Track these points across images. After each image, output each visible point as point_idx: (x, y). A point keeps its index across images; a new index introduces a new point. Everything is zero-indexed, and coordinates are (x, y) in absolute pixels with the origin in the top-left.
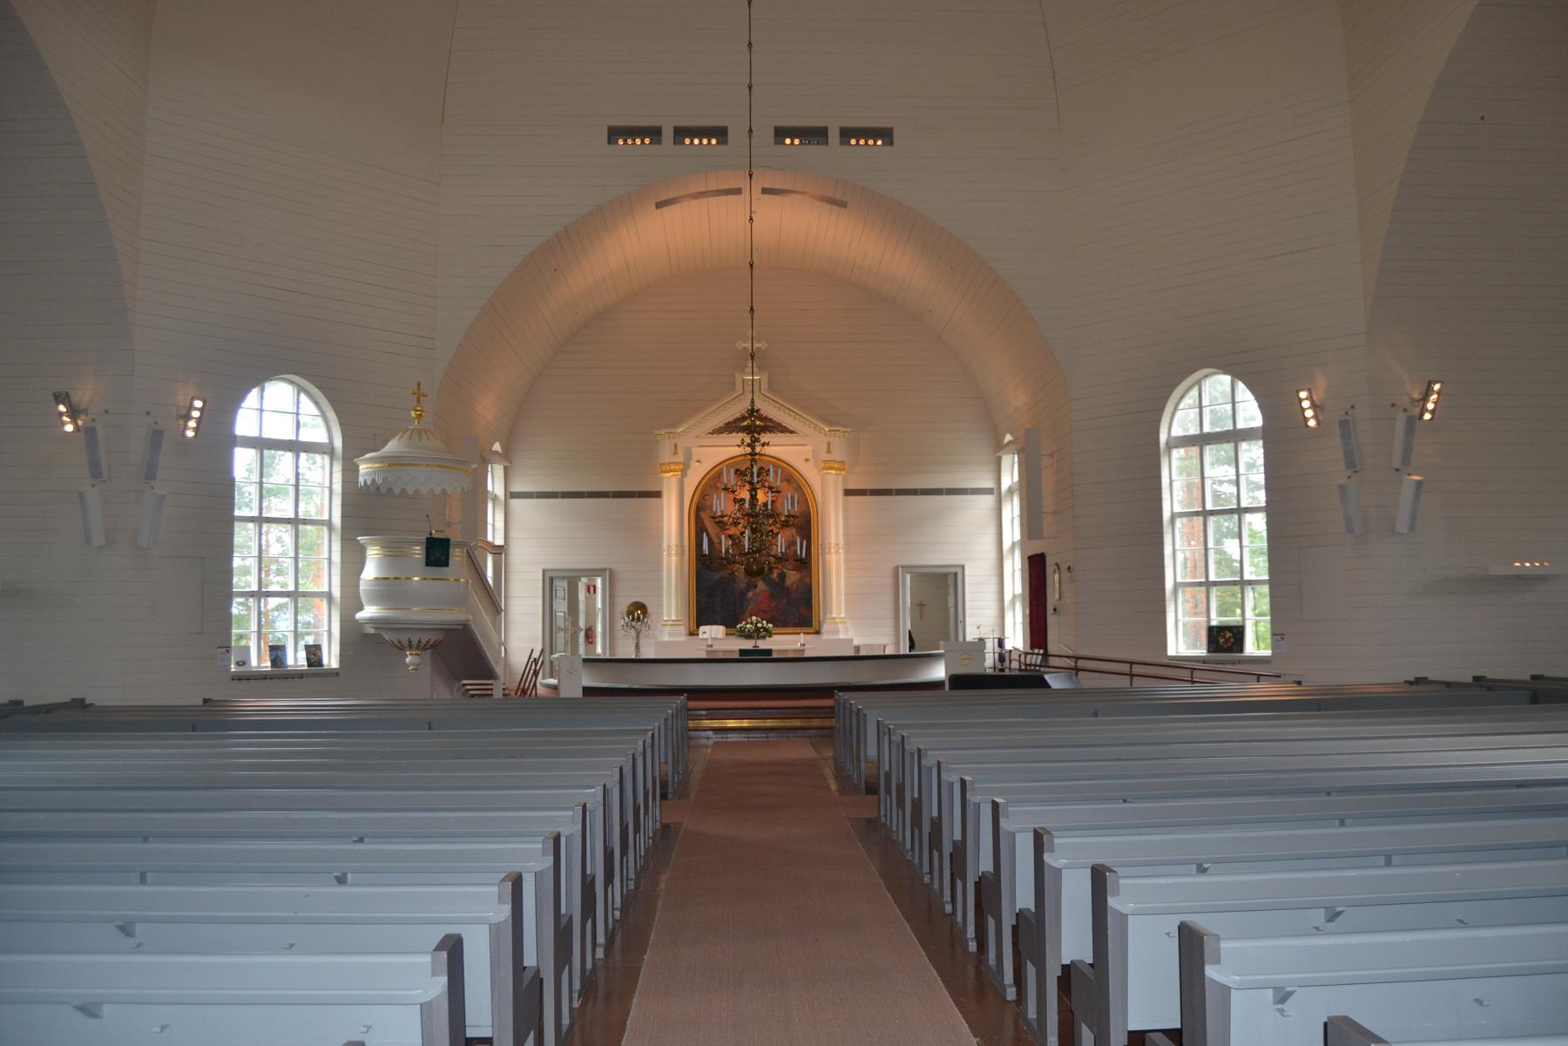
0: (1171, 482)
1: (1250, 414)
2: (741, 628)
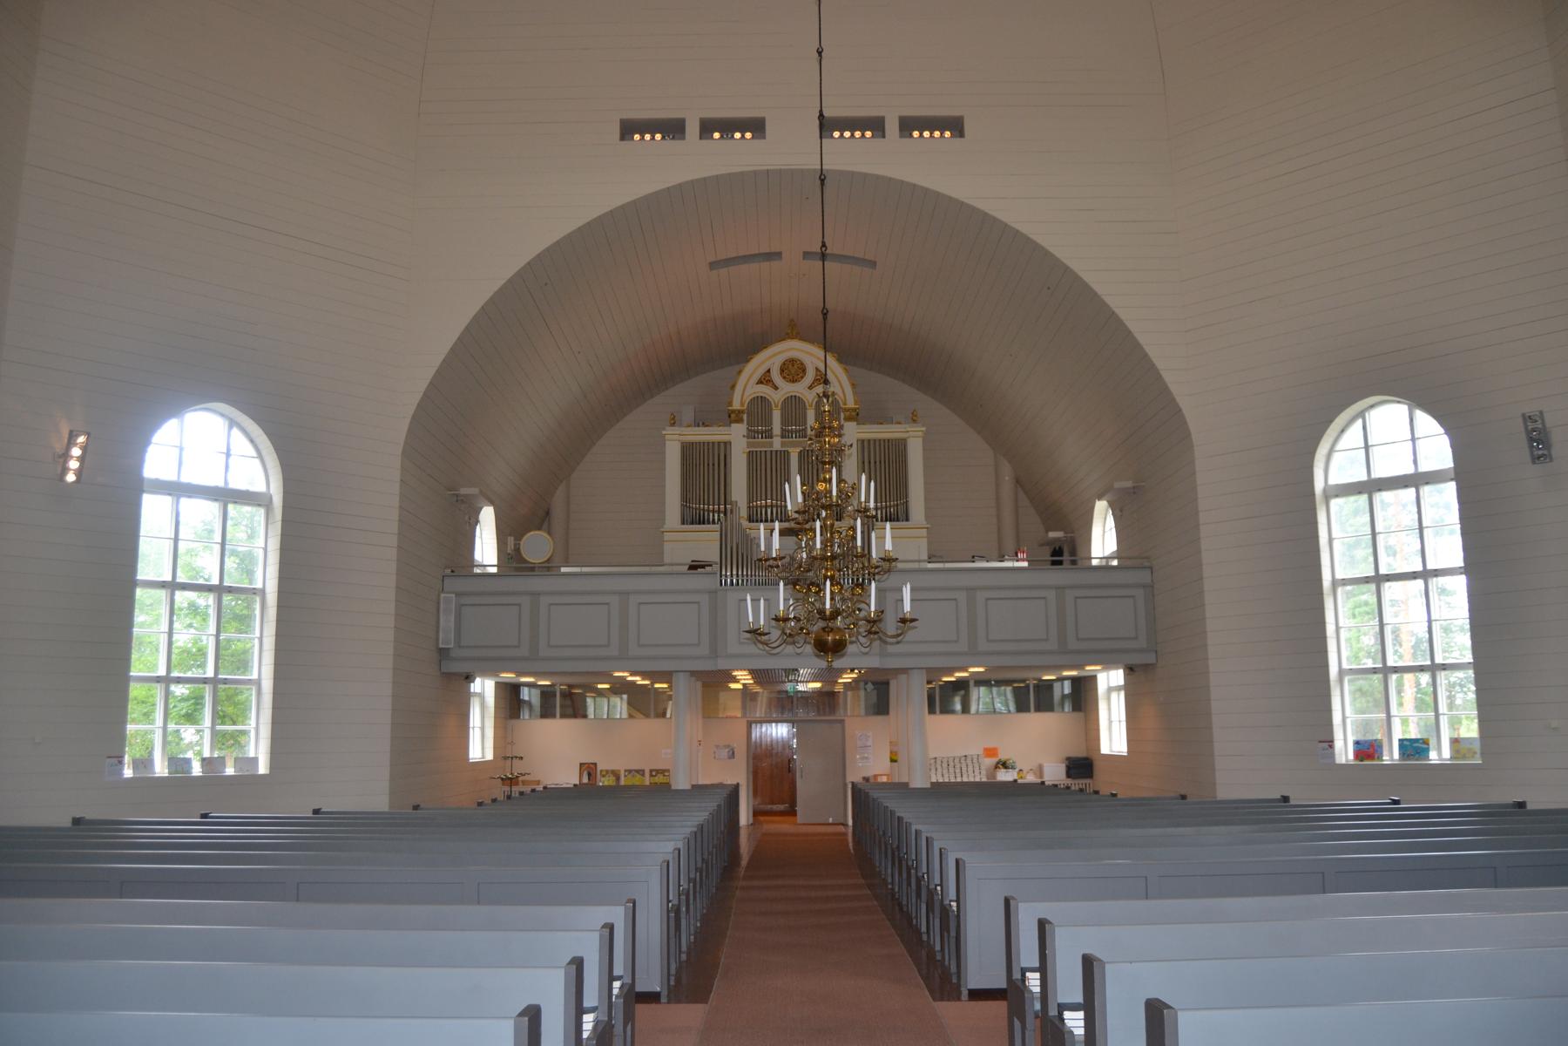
0: (1331, 540)
1: (1437, 450)
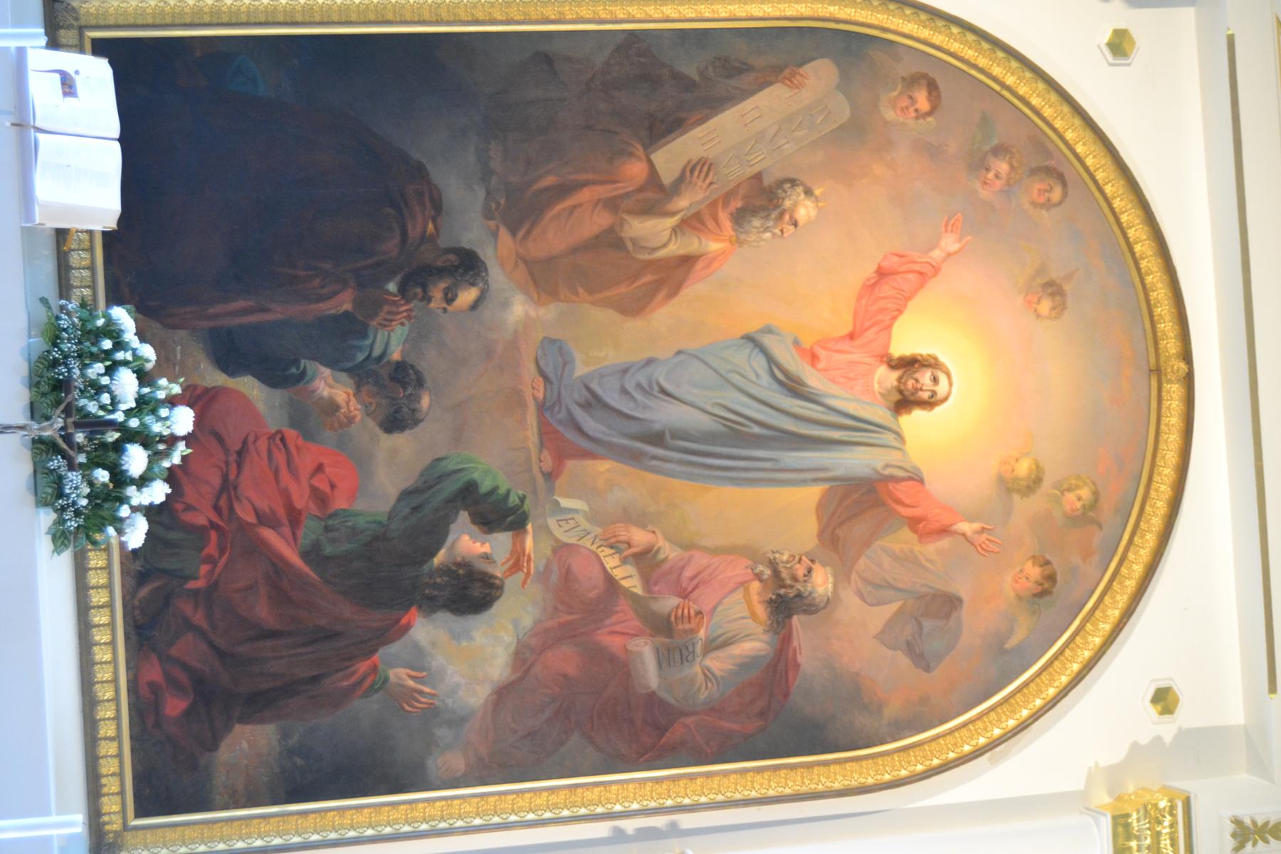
2: (112, 331)
